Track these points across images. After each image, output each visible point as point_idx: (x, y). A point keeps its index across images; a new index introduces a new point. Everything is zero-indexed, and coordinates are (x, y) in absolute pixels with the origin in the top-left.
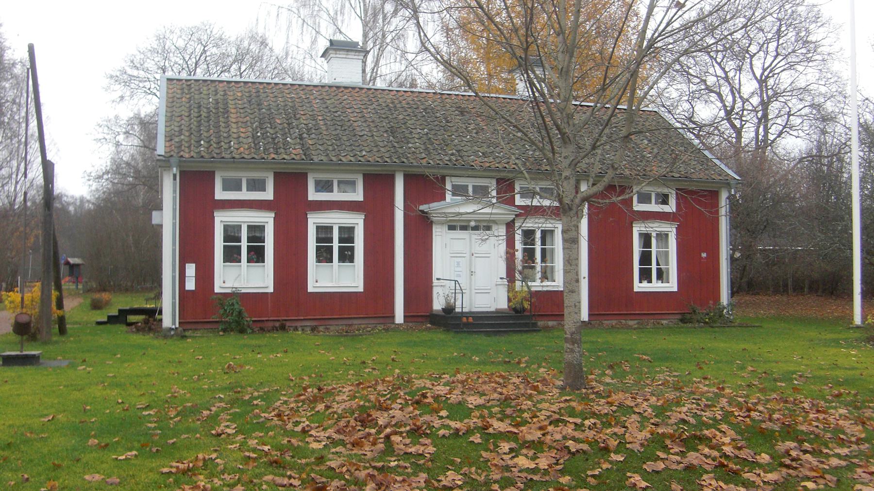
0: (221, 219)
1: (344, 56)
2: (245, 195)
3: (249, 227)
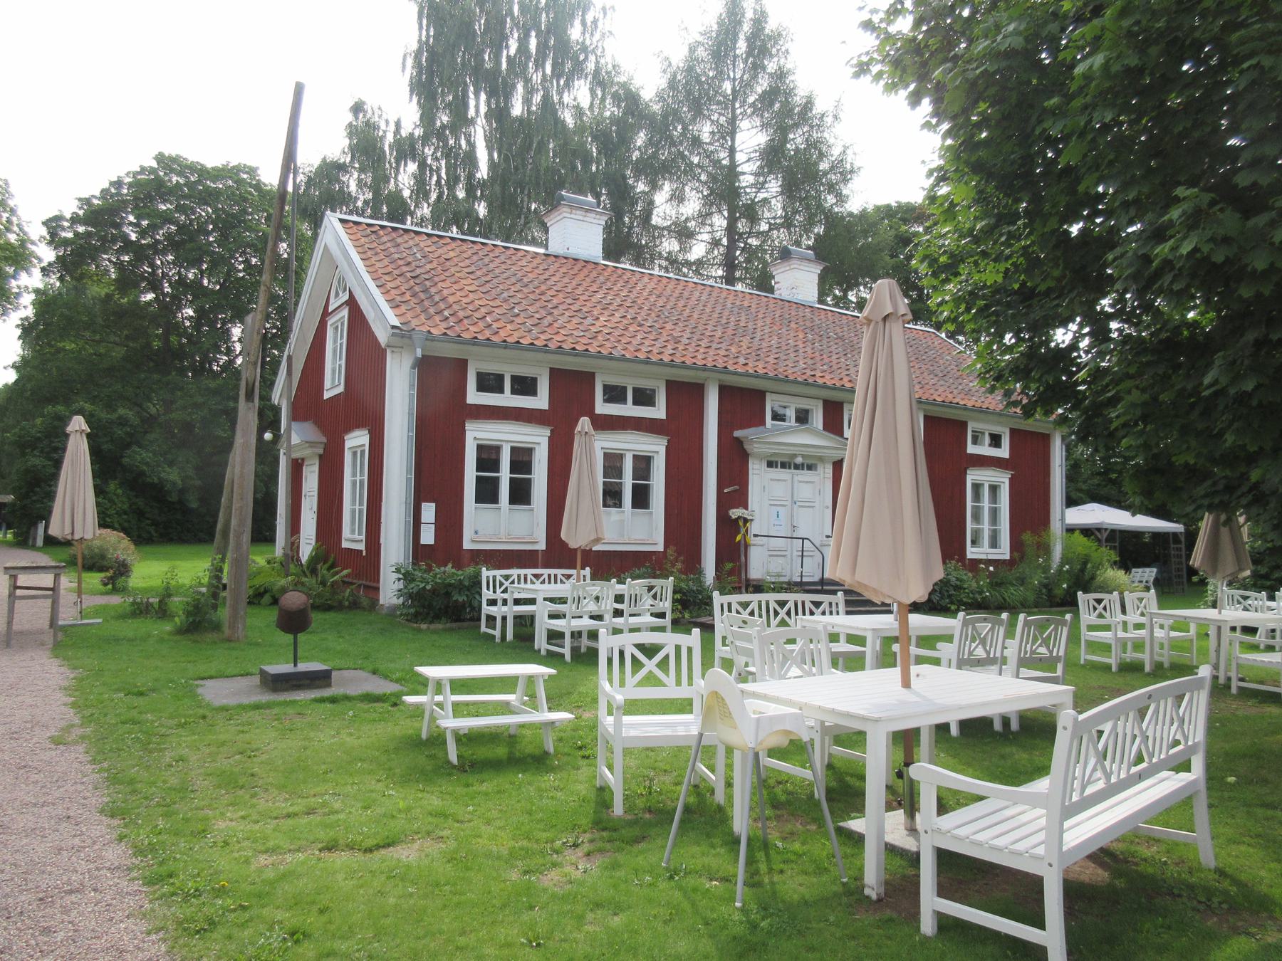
0: (476, 434)
1: (581, 218)
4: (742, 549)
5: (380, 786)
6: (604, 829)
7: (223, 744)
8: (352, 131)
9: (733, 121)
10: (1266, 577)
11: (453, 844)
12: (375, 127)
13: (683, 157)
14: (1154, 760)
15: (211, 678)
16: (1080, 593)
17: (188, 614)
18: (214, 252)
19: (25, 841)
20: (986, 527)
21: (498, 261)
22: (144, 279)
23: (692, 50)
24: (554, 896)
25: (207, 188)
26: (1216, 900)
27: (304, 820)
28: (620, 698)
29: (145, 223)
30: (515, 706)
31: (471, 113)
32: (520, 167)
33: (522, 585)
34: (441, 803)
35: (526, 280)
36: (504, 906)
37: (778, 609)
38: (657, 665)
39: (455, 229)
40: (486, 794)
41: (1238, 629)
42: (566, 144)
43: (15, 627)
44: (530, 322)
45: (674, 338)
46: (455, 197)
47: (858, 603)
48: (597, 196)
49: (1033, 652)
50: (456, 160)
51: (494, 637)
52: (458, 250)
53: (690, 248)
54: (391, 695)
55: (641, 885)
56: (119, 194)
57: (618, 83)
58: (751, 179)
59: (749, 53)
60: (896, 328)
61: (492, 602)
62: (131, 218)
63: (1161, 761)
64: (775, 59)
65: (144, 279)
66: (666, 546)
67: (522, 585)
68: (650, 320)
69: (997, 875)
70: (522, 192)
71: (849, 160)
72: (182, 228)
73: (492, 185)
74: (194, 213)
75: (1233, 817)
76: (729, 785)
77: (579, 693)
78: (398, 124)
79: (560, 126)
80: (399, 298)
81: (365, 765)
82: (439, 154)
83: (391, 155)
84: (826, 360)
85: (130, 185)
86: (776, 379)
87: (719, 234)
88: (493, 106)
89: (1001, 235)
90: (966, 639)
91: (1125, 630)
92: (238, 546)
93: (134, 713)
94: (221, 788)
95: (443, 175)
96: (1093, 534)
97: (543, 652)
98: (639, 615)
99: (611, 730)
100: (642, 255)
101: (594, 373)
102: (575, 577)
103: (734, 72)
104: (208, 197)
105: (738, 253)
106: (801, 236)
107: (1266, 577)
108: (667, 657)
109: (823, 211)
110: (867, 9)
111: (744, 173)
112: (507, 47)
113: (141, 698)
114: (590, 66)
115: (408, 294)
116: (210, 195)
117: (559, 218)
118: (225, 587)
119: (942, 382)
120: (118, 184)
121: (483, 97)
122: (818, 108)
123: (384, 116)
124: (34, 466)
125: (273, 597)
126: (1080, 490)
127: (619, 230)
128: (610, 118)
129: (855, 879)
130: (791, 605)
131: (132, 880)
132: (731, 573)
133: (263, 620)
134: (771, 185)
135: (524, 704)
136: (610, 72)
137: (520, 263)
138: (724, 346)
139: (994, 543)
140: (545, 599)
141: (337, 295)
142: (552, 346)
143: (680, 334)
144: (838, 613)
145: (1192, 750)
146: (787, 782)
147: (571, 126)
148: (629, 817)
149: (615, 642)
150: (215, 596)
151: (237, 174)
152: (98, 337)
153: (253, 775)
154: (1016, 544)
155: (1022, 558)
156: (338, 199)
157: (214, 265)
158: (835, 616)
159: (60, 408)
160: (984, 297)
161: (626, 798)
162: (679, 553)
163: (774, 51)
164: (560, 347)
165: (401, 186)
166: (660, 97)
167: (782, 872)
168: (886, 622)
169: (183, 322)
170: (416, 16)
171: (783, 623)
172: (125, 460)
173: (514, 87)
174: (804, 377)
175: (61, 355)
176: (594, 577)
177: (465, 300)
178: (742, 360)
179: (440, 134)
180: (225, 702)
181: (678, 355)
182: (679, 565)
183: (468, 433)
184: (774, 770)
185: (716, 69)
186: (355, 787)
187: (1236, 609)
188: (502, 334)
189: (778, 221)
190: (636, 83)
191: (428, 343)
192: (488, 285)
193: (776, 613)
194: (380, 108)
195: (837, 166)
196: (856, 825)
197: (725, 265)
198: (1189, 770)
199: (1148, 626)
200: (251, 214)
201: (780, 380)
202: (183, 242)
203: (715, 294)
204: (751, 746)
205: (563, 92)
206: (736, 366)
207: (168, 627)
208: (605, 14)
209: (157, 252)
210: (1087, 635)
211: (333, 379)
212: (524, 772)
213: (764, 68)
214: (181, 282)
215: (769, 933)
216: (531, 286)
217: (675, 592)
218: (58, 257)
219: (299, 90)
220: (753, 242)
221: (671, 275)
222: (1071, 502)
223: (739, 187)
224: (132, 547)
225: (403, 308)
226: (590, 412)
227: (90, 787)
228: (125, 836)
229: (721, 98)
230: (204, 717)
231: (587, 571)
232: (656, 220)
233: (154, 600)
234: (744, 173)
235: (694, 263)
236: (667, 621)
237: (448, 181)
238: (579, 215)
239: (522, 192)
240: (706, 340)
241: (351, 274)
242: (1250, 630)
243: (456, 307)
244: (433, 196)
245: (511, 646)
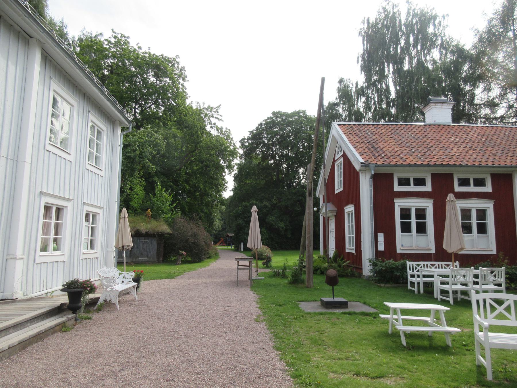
0: (399, 204)
1: (440, 107)
2: (472, 188)
5: (374, 351)
7: (311, 327)
8: (339, 90)
11: (409, 382)
12: (348, 87)
13: (489, 71)
15: (303, 301)
17: (293, 276)
18: (292, 143)
19: (251, 355)
21: (403, 131)
22: (270, 156)
23: (490, 22)
25: (289, 121)
27: (345, 362)
28: (486, 324)
29: (269, 136)
30: (430, 323)
31: (386, 73)
32: (409, 90)
34: (401, 362)
35: (416, 137)
39: (382, 120)
42: (429, 77)
43: (239, 279)
45: (493, 154)
46: (382, 108)
48: (446, 96)
51: (414, 291)
52: (385, 129)
54: (373, 313)
56: (261, 128)
61: (413, 276)
62: (265, 135)
65: (270, 156)
67: (426, 269)
68: (479, 147)
70: (411, 101)
72: (281, 136)
73: (397, 100)
74: (285, 130)
77: (460, 320)
78: (357, 84)
79: (426, 70)
80: (363, 152)
81: (366, 342)
82: (374, 92)
83: (355, 96)
85: (265, 124)
87: (512, 102)
88: (395, 68)
92: (309, 251)
93: (279, 313)
94: (312, 344)
95: (376, 100)
97: (439, 300)
98: (487, 284)
102: (451, 265)
104: (289, 124)
112: (400, 44)
113: (280, 307)
114: (439, 42)
115: (366, 149)
116: (290, 123)
118: (304, 267)
120: (261, 124)
121: (391, 65)
123: (351, 82)
124: (240, 223)
125: (321, 271)
128: (450, 61)
131: (287, 375)
133: (319, 280)
136: (448, 42)
137: (413, 130)
140: (438, 275)
141: (338, 153)
143: (496, 152)
148: (495, 382)
149: (481, 297)
150: (301, 270)
151: (299, 114)
152: (256, 178)
153: (323, 341)
156: (335, 117)
157: (292, 148)
159: (247, 203)
161: (493, 372)
164: (435, 164)
165: (359, 107)
166: (475, 47)
169: (283, 170)
170: (362, 41)
172: (267, 220)
173: (404, 58)
175: (246, 185)
176: (461, 266)
179: (374, 84)
180: (309, 311)
181: (496, 161)
182: (506, 261)
183: (395, 204)
186: (364, 351)
188: (408, 161)
190: (462, 43)
191: (377, 168)
194: (349, 79)
200: (304, 127)
202: (282, 141)
205: (426, 56)
207: (286, 281)
208: (444, 18)
209: (274, 146)
211: (338, 186)
212: (438, 353)
214: (282, 155)
216: (419, 139)
218: (244, 152)
219: (323, 80)
221: (487, 125)
224: (271, 251)
225: (365, 155)
226: (452, 191)
227: (269, 338)
228: (283, 358)
230: (303, 316)
231: (457, 263)
232: (476, 101)
233: (281, 271)
235: (499, 118)
236: (503, 287)
237: (378, 102)
238: (439, 106)
239: (411, 101)
240: (511, 153)
241: (343, 145)
243: (387, 152)
244: (373, 109)
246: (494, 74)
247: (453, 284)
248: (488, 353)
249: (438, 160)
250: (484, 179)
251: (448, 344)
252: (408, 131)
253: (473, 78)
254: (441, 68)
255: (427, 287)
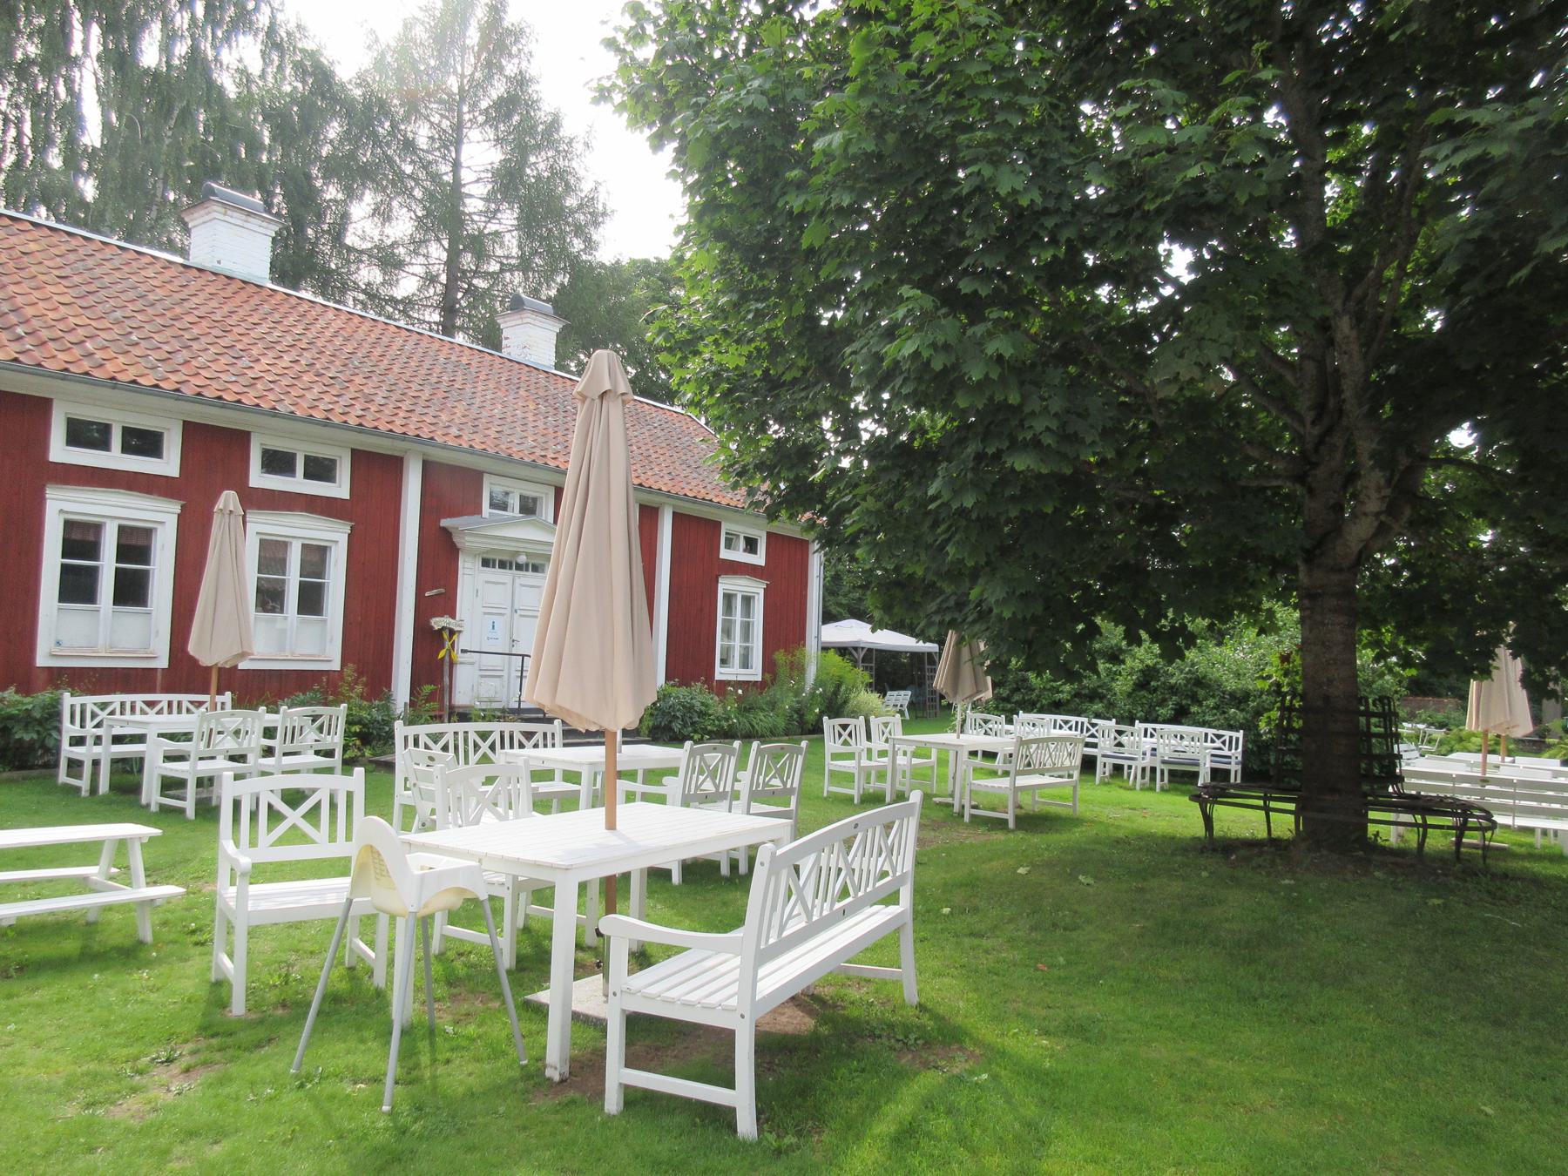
2: (298, 484)
3: (122, 529)
4: (446, 668)
6: (212, 1036)
9: (458, 127)
10: (1007, 700)
14: (860, 894)
16: (825, 718)
20: (737, 643)
21: (108, 265)
23: (408, 26)
24: (129, 1130)
26: (912, 1037)
28: (245, 861)
30: (96, 882)
31: (76, 49)
33: (128, 716)
35: (151, 297)
36: (48, 1154)
37: (479, 741)
38: (304, 817)
39: (43, 210)
40: (38, 1006)
41: (980, 754)
42: (223, 119)
44: (154, 355)
47: (573, 736)
49: (766, 784)
50: (48, 113)
51: (78, 789)
52: (44, 242)
53: (397, 280)
55: (258, 1102)
57: (303, 51)
58: (480, 205)
59: (483, 45)
60: (614, 410)
61: (78, 741)
63: (866, 894)
64: (516, 61)
66: (343, 664)
67: (128, 716)
68: (333, 369)
69: (699, 1037)
70: (154, 174)
71: (601, 200)
75: (943, 949)
76: (391, 963)
77: (202, 860)
84: (560, 439)
86: (496, 457)
89: (749, 312)
90: (693, 772)
91: (869, 758)
95: (27, 128)
96: (851, 654)
97: (154, 808)
99: (232, 904)
100: (332, 284)
101: (248, 433)
103: (463, 68)
105: (460, 295)
106: (540, 284)
107: (1007, 700)
108: (317, 806)
109: (569, 255)
110: (611, 25)
111: (471, 196)
114: (263, 20)
117: (206, 218)
119: (695, 475)
121: (95, 30)
122: (566, 131)
126: (839, 605)
127: (298, 247)
129: (537, 1060)
130: (496, 736)
132: (431, 697)
134: (505, 216)
135: (111, 878)
137: (143, 273)
138: (431, 411)
139: (745, 664)
140: (160, 735)
142: (188, 391)
143: (373, 391)
144: (553, 745)
145: (901, 880)
146: (470, 952)
147: (232, 96)
148: (254, 1017)
154: (769, 665)
155: (773, 681)
158: (549, 749)
160: (728, 380)
161: (251, 992)
162: (360, 673)
163: (514, 50)
166: (362, 81)
167: (448, 1061)
168: (596, 753)
171: (485, 759)
174: (533, 457)
176: (237, 704)
177: (51, 315)
178: (454, 431)
181: (369, 417)
184: (454, 939)
185: (439, 57)
187: (978, 734)
189: (513, 261)
192: (91, 297)
193: (477, 747)
195: (587, 204)
196: (542, 996)
197: (443, 309)
198: (897, 903)
199: (890, 753)
201: (502, 459)
203: (424, 344)
204: (412, 910)
206: (445, 438)
210: (832, 765)
212: (101, 971)
213: (501, 69)
215: (421, 1138)
216: (159, 306)
217: (349, 723)
220: (481, 283)
221: (371, 314)
222: (828, 617)
223: (463, 213)
229: (444, 96)
232: (350, 239)
234: (471, 196)
235: (402, 301)
236: (337, 759)
237: (33, 143)
238: (237, 217)
239: (154, 174)
240: (408, 402)
242: (990, 755)
245: (105, 801)
246: (400, 175)
247: (201, 759)
248: (240, 941)
249: (208, 382)
250: (333, 462)
251: (141, 936)
252: (126, 269)
253: (348, 167)
254: (262, 104)
255: (127, 772)
